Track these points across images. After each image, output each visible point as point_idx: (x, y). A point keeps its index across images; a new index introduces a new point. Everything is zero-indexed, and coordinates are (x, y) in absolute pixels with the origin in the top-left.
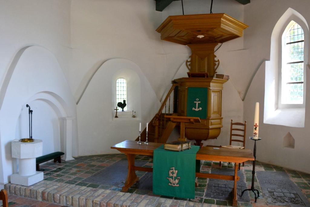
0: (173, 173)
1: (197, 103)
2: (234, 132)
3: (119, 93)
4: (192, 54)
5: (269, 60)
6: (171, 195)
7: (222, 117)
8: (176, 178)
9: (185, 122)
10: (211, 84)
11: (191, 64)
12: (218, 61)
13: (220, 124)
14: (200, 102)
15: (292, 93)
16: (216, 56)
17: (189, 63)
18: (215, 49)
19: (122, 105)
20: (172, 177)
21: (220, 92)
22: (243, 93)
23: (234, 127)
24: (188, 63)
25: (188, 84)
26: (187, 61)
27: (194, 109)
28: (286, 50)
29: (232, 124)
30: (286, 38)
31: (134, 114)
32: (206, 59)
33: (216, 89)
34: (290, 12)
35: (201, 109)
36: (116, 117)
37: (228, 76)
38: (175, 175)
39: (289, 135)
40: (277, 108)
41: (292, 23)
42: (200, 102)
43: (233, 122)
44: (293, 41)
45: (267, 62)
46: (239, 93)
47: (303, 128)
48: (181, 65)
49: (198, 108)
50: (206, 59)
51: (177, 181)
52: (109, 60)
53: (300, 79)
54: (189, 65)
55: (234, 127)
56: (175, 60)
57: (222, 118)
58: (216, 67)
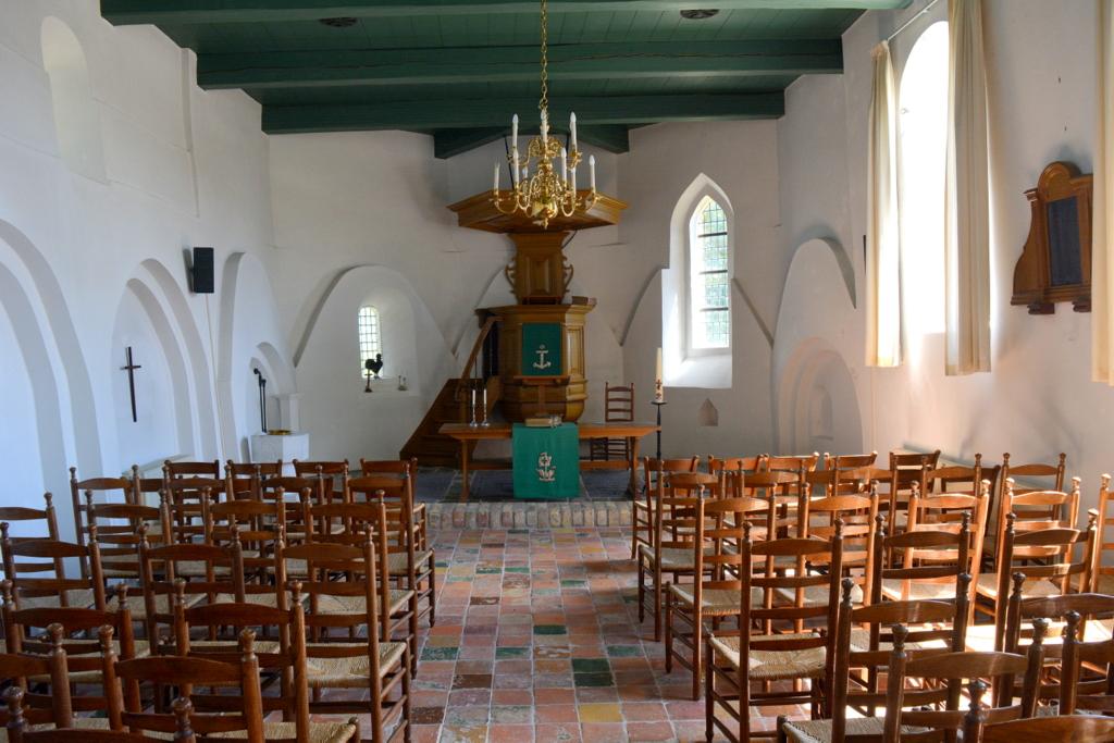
0: (545, 461)
1: (542, 354)
2: (612, 405)
3: (374, 336)
4: (518, 255)
5: (668, 267)
6: (543, 496)
7: (587, 378)
8: (549, 468)
9: (546, 386)
10: (567, 316)
11: (516, 276)
12: (571, 267)
13: (583, 392)
14: (546, 352)
15: (709, 328)
16: (565, 258)
17: (512, 272)
18: (564, 243)
19: (374, 365)
20: (543, 468)
21: (581, 331)
22: (620, 330)
23: (612, 395)
24: (510, 273)
25: (522, 319)
26: (507, 269)
27: (536, 365)
28: (698, 247)
29: (608, 390)
30: (697, 227)
31: (402, 383)
32: (547, 263)
33: (577, 325)
34: (701, 180)
35: (549, 364)
36: (368, 390)
37: (594, 300)
38: (548, 464)
39: (709, 406)
40: (685, 357)
41: (707, 198)
42: (546, 352)
43: (609, 386)
44: (709, 233)
45: (664, 271)
46: (614, 331)
47: (729, 390)
48: (495, 275)
49: (545, 363)
50: (547, 263)
51: (551, 473)
52: (352, 271)
53: (723, 303)
54: (513, 276)
55: (612, 395)
56: (481, 267)
57: (586, 381)
58: (566, 280)
